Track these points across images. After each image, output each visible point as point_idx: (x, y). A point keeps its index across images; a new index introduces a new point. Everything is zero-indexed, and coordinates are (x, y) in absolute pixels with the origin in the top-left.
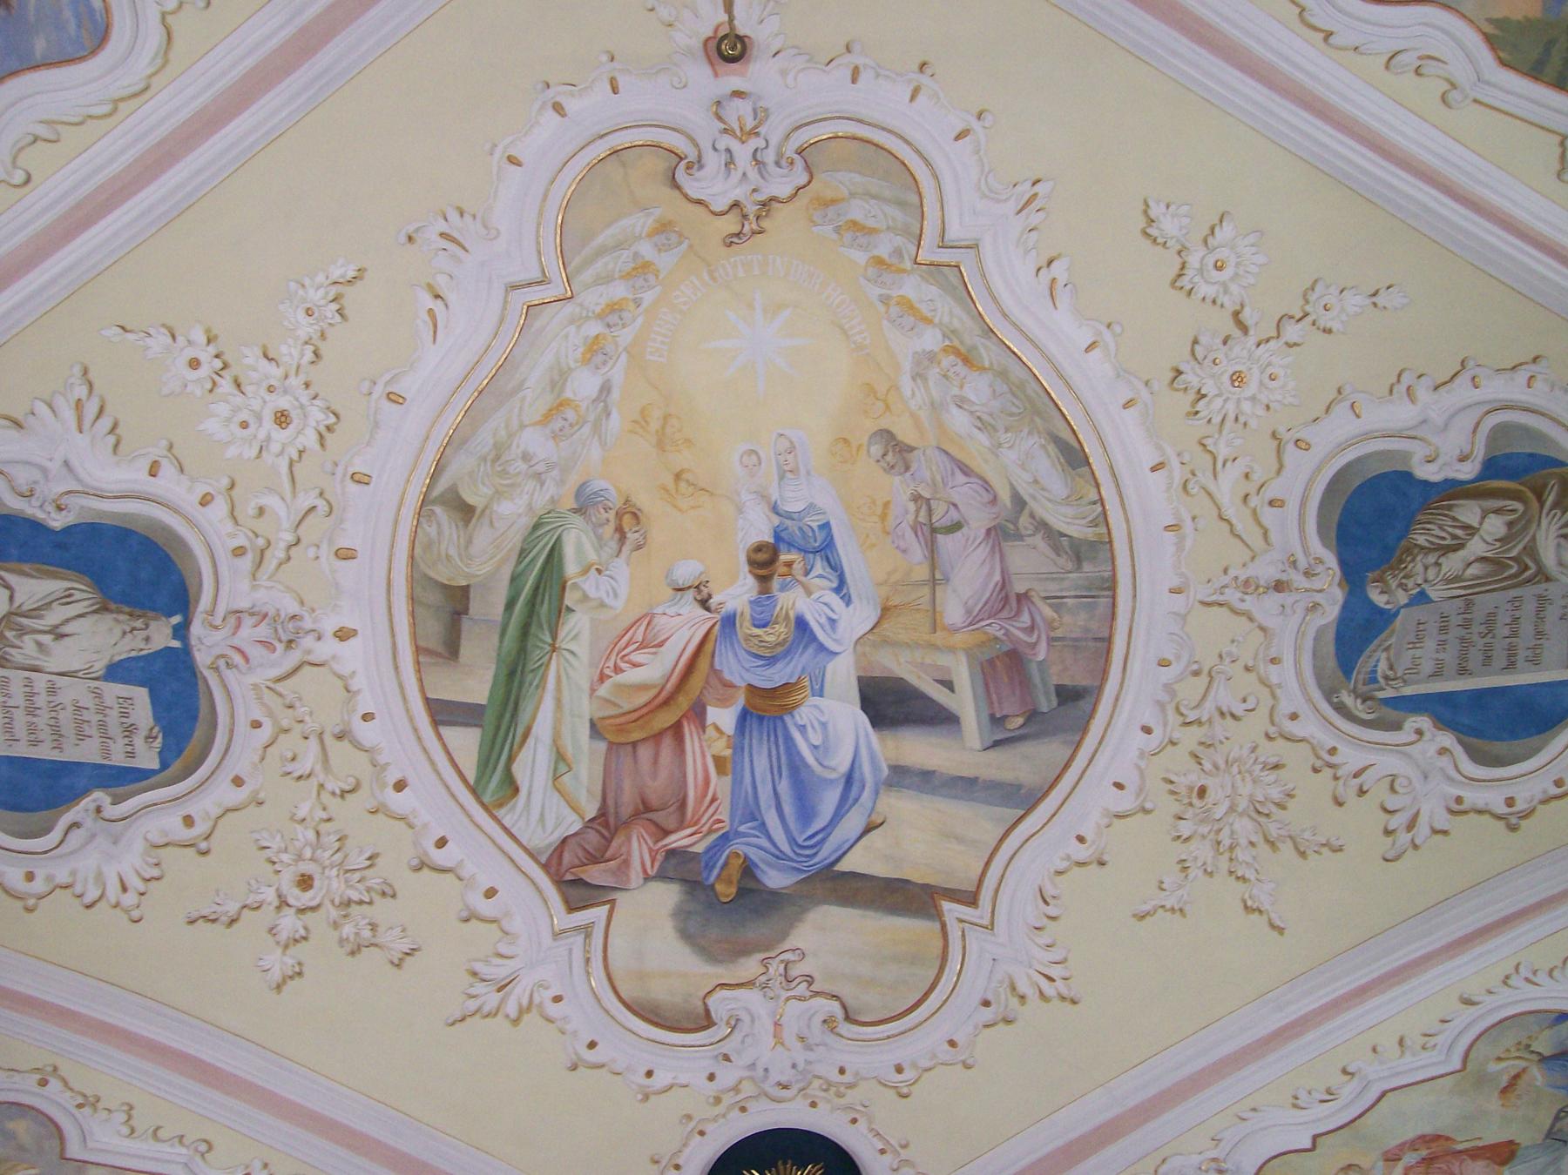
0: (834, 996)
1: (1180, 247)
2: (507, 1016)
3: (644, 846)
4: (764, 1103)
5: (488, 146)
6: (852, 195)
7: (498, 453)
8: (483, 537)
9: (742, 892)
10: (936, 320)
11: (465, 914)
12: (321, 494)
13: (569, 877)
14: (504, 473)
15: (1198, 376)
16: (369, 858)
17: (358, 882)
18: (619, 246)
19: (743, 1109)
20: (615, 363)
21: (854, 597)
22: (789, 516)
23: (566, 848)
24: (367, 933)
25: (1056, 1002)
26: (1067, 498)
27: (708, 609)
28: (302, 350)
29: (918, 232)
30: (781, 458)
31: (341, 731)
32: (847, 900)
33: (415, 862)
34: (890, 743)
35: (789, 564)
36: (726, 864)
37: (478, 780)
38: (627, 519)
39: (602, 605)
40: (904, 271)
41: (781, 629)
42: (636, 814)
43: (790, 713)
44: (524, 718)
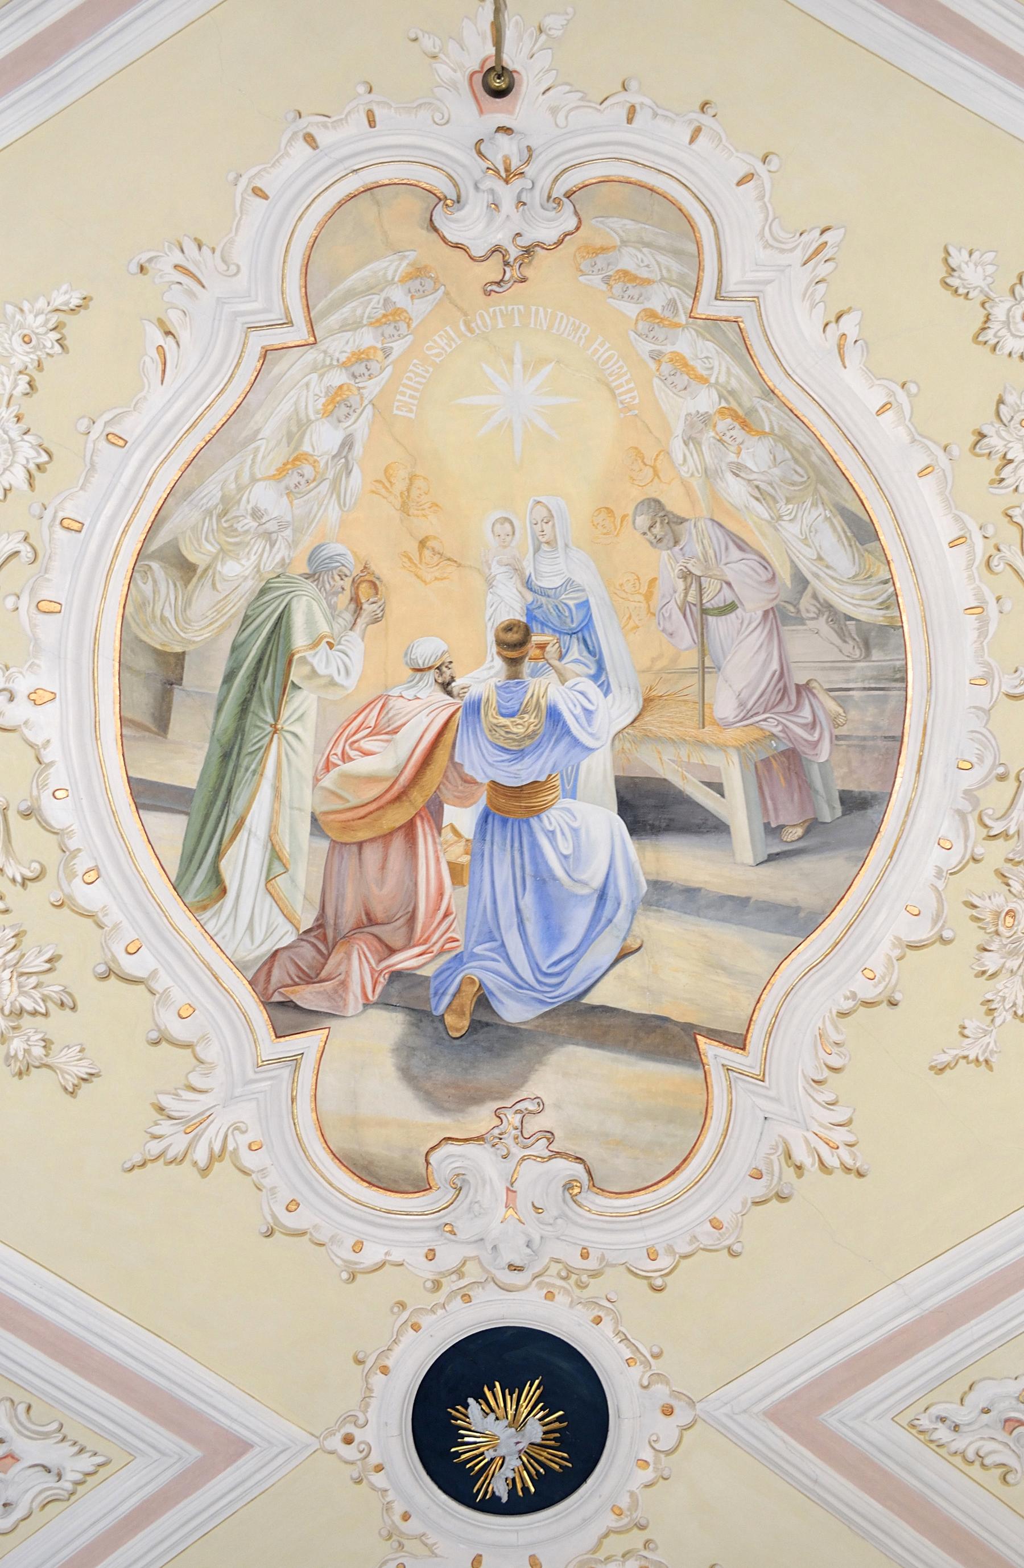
0: (578, 1158)
1: (982, 298)
2: (195, 1163)
3: (366, 965)
4: (492, 1292)
5: (231, 176)
6: (624, 243)
7: (227, 505)
8: (203, 599)
9: (476, 1026)
10: (713, 380)
11: (154, 1035)
12: (26, 539)
13: (277, 998)
14: (231, 530)
15: (1003, 439)
16: (49, 961)
17: (34, 988)
18: (370, 290)
19: (467, 1298)
20: (358, 418)
21: (614, 686)
22: (543, 592)
23: (276, 964)
24: (38, 1051)
25: (839, 1173)
26: (854, 577)
27: (450, 694)
28: (15, 380)
29: (695, 284)
30: (538, 528)
31: (28, 809)
32: (597, 1039)
33: (102, 969)
34: (650, 854)
35: (542, 647)
36: (459, 991)
37: (181, 877)
38: (364, 588)
39: (332, 683)
40: (677, 325)
41: (530, 719)
42: (359, 927)
43: (538, 816)
44: (237, 805)
